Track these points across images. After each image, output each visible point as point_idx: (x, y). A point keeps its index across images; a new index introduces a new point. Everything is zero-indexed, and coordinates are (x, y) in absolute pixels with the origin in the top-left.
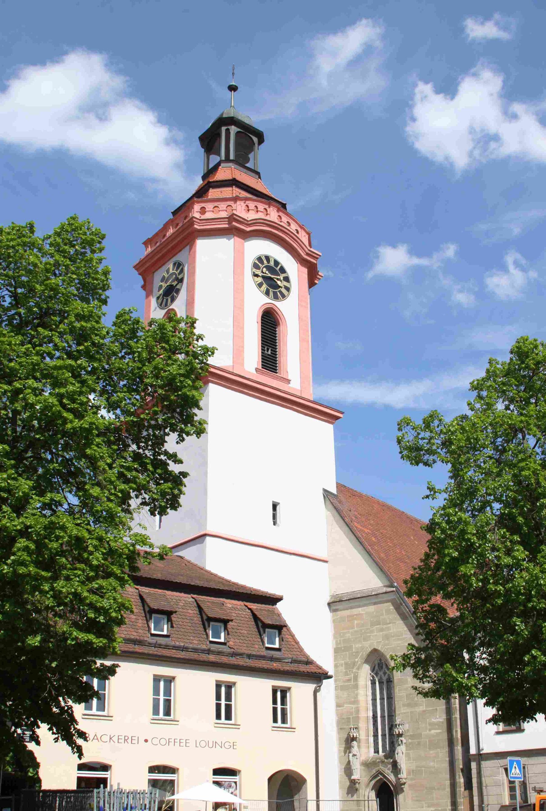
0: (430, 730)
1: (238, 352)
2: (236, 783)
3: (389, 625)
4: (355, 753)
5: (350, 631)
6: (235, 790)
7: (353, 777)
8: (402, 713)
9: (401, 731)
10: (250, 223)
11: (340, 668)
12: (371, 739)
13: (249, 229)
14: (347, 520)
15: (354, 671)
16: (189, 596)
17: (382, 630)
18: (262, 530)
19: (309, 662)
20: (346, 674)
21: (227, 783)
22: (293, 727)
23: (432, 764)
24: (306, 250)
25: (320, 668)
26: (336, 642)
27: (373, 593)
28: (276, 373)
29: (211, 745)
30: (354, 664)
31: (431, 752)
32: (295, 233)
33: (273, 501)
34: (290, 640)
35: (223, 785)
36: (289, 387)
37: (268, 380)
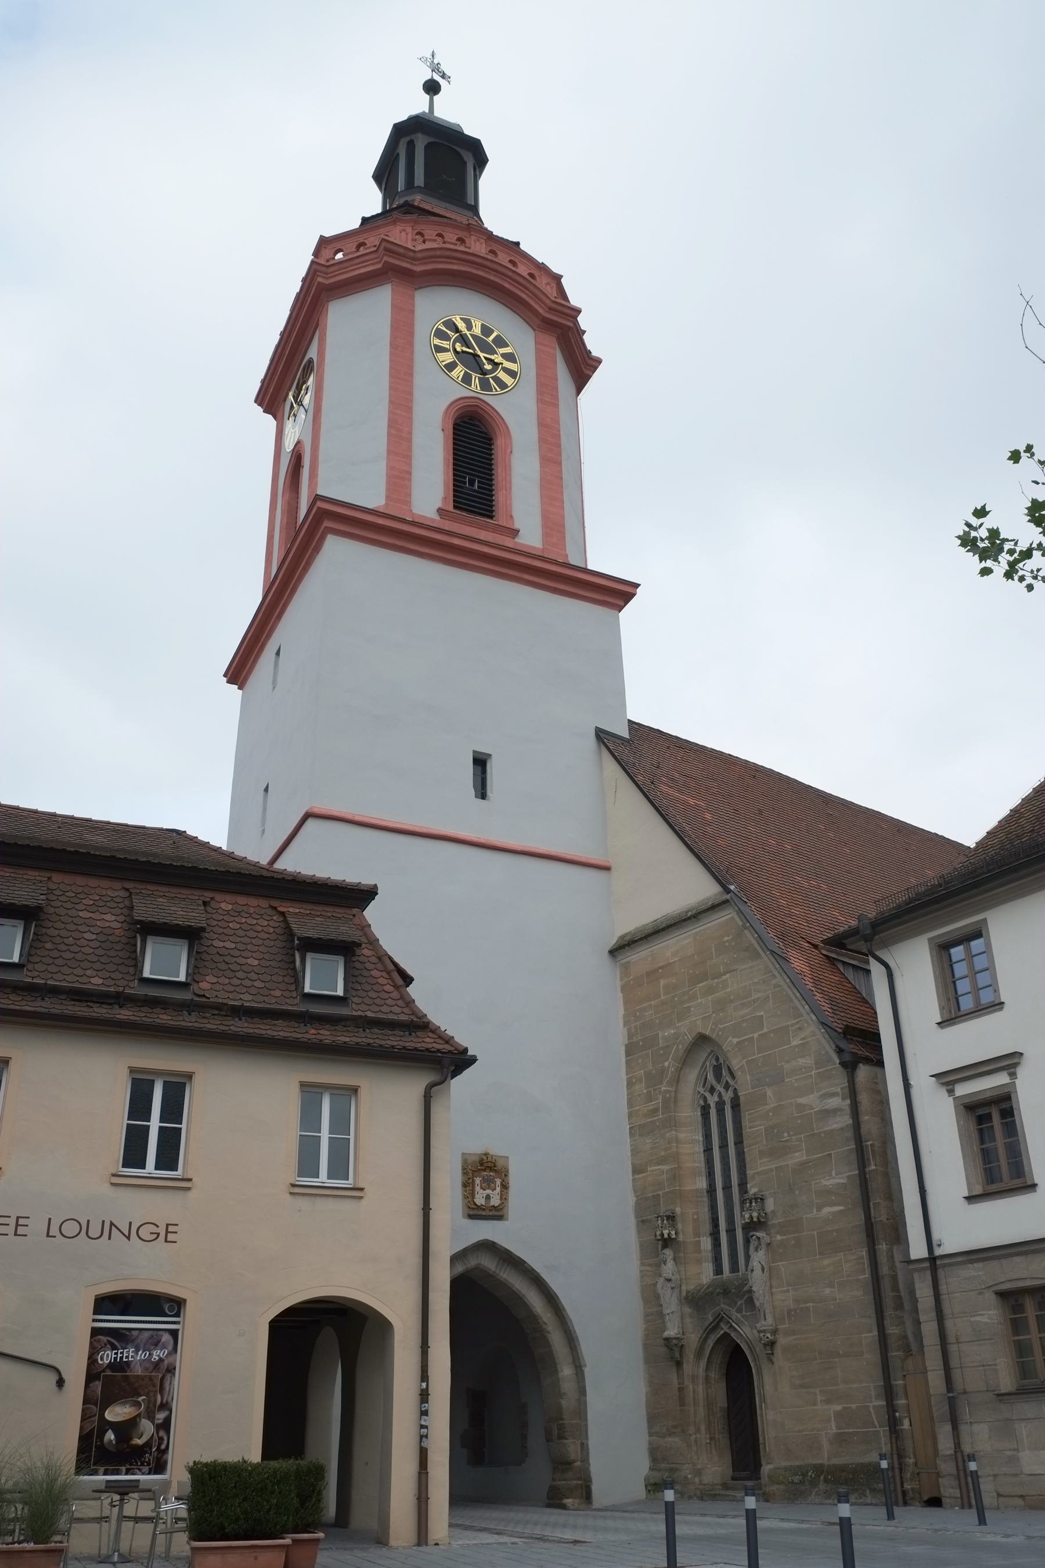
0: (819, 1209)
1: (399, 479)
2: (174, 1334)
3: (724, 977)
4: (670, 1276)
5: (653, 1003)
6: (169, 1354)
7: (666, 1334)
8: (758, 1173)
9: (755, 1214)
10: (419, 255)
11: (637, 1087)
12: (706, 1243)
13: (418, 269)
14: (639, 778)
15: (663, 1089)
16: (118, 885)
17: (710, 991)
18: (459, 811)
19: (421, 1025)
20: (649, 1098)
21: (147, 1334)
22: (361, 1186)
23: (828, 1291)
24: (548, 302)
25: (449, 1040)
26: (629, 1031)
27: (689, 914)
28: (491, 517)
29: (95, 1231)
30: (663, 1071)
31: (826, 1262)
32: (510, 266)
33: (474, 752)
34: (382, 981)
35: (133, 1341)
36: (516, 543)
37: (469, 530)
